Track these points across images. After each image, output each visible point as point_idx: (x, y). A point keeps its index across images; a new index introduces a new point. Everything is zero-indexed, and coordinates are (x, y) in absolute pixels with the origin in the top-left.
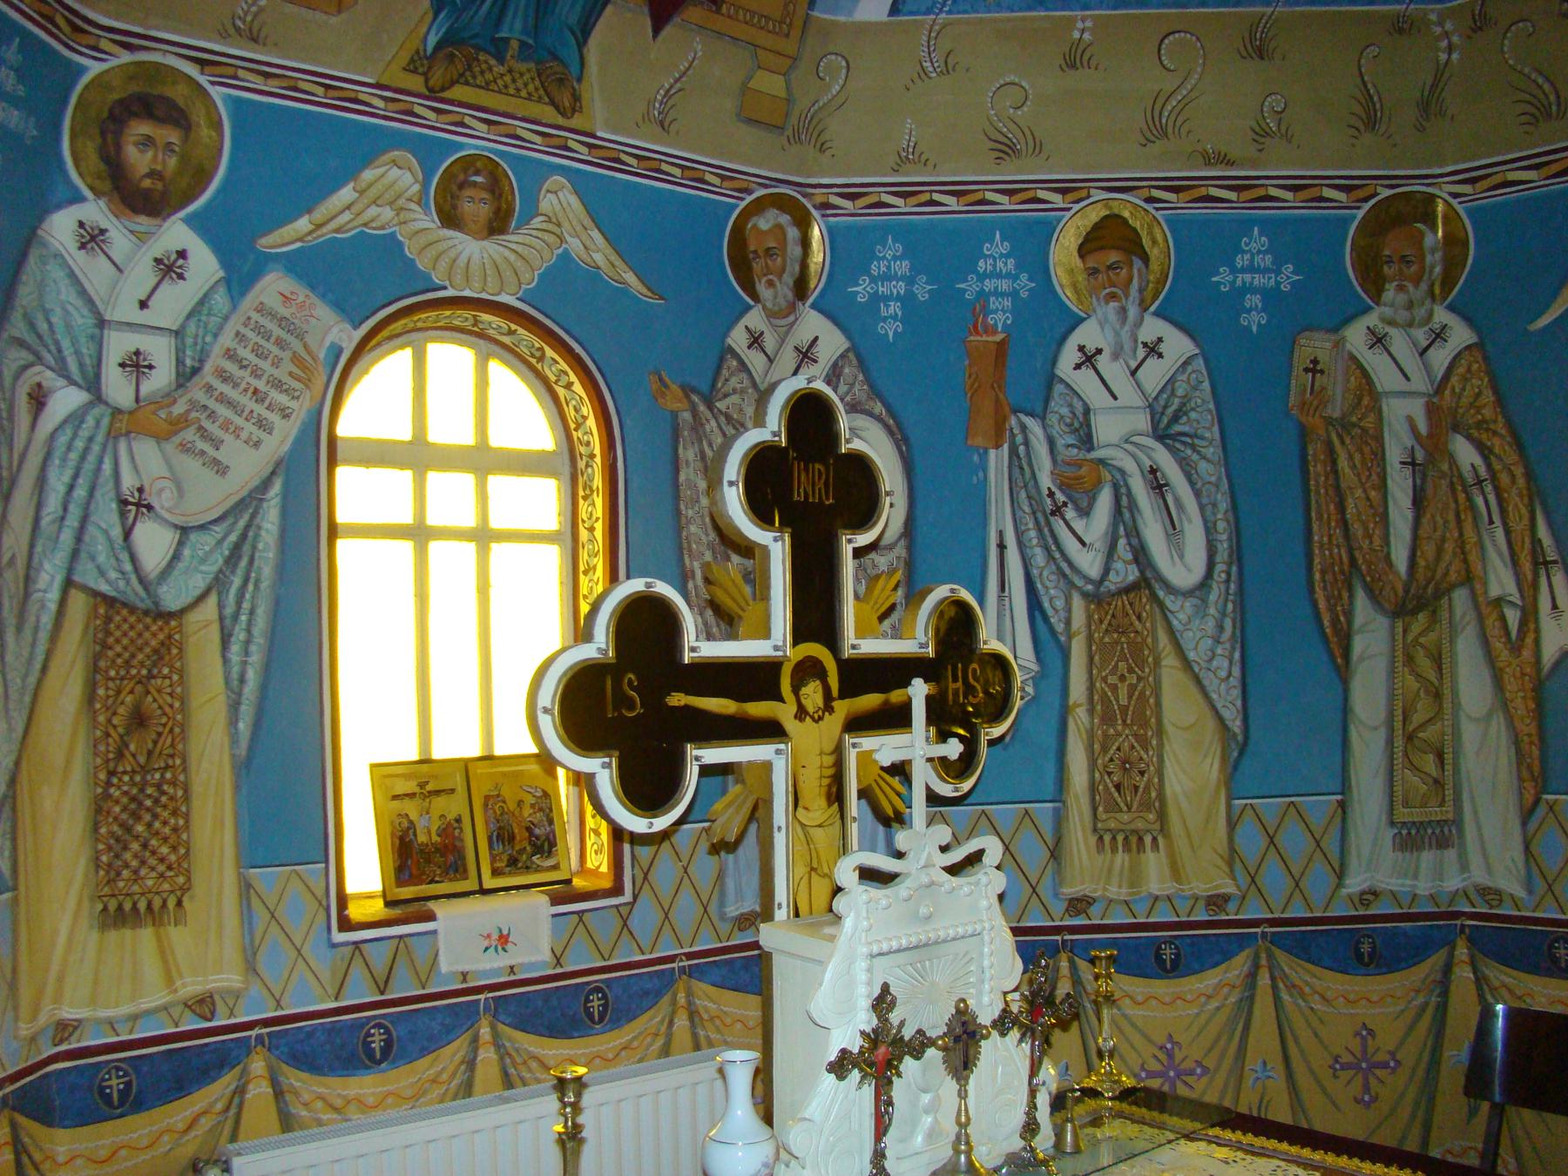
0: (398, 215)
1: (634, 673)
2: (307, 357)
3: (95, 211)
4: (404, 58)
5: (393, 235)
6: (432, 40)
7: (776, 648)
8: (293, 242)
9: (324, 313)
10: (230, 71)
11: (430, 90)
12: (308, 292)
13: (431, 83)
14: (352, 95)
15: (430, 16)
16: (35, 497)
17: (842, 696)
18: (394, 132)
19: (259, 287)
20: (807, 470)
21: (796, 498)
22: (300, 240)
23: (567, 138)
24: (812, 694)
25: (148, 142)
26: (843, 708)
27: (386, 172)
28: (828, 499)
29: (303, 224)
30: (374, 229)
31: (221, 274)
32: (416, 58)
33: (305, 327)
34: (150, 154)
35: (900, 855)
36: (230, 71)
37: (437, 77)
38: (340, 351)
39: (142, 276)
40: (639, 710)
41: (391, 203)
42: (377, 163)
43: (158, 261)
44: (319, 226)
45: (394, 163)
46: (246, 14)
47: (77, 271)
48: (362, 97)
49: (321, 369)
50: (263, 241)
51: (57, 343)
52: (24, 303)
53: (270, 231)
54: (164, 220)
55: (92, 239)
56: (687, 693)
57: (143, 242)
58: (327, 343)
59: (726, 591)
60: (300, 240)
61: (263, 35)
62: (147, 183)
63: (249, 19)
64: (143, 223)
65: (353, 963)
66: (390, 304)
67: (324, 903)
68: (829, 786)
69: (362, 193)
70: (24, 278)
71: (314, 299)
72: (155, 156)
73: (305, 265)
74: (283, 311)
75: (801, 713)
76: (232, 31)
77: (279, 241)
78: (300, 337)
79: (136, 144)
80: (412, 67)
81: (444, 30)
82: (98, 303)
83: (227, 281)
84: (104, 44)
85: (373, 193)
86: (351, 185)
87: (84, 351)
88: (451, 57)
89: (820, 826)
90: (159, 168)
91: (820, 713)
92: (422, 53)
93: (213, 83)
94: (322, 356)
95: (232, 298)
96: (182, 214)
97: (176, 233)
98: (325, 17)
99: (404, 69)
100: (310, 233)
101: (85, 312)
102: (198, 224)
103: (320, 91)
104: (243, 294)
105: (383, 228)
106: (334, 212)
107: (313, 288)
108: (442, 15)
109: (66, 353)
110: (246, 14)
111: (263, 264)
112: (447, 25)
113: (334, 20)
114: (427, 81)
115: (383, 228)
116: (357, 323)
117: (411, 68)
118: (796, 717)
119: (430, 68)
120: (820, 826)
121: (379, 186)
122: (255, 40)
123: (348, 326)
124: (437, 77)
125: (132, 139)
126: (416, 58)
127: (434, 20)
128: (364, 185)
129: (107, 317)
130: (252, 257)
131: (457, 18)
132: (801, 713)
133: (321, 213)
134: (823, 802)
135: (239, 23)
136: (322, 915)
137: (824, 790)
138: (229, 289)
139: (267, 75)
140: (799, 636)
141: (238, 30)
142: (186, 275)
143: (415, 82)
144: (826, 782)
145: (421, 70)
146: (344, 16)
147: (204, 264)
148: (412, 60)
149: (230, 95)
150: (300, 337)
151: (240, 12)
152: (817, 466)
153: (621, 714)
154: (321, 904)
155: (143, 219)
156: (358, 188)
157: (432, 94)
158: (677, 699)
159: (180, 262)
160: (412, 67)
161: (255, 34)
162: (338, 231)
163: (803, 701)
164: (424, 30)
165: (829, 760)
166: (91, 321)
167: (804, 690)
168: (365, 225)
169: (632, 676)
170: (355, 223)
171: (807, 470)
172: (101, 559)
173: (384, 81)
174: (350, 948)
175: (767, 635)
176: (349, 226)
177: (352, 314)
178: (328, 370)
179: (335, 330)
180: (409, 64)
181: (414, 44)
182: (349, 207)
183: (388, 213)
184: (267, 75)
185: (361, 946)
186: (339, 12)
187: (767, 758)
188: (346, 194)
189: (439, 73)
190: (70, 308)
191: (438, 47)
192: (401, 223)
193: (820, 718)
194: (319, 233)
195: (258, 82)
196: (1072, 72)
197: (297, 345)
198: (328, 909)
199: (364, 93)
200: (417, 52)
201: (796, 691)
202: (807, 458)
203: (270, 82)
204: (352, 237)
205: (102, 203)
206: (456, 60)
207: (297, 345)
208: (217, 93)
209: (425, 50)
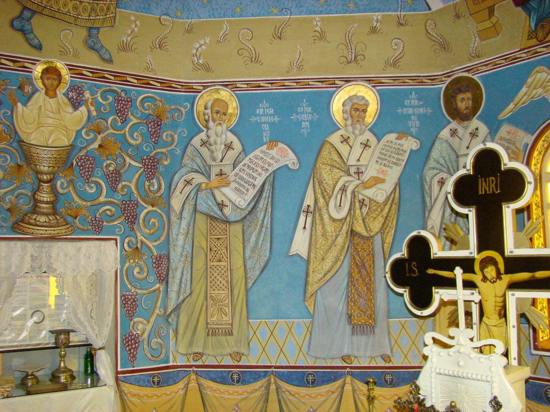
0: (544, 89)
1: (415, 261)
2: (516, 150)
3: (454, 125)
4: (526, 36)
5: (544, 97)
6: (533, 25)
7: (471, 253)
8: (508, 113)
9: (521, 133)
10: (476, 69)
11: (540, 41)
12: (515, 128)
13: (539, 39)
14: (514, 57)
15: (528, 17)
16: (442, 210)
17: (506, 272)
18: (533, 62)
19: (499, 132)
20: (485, 181)
21: (480, 193)
22: (511, 111)
23: (536, 49)
24: (490, 272)
25: (463, 99)
26: (507, 279)
27: (535, 77)
28: (497, 190)
29: (511, 106)
30: (537, 97)
31: (488, 131)
32: (530, 34)
33: (515, 140)
34: (464, 103)
35: (452, 338)
36: (476, 69)
37: (541, 35)
38: (528, 145)
39: (467, 138)
40: (417, 274)
41: (541, 86)
42: (532, 75)
43: (471, 133)
44: (516, 105)
45: (538, 72)
46: (473, 51)
47: (451, 143)
48: (517, 56)
49: (521, 153)
50: (500, 116)
51: (447, 165)
52: (434, 157)
53: (500, 114)
54: (471, 120)
55: (454, 133)
56: (435, 269)
57: (466, 129)
58: (523, 143)
59: (453, 233)
60: (511, 111)
61: (480, 54)
62: (465, 111)
63: (474, 52)
64: (466, 123)
65: (540, 362)
66: (544, 123)
67: (528, 338)
68: (500, 310)
69: (529, 87)
70: (433, 150)
71: (518, 130)
72: (466, 103)
73: (513, 120)
74: (508, 137)
75: (485, 279)
76: (471, 58)
77: (505, 114)
78: (514, 144)
79: (460, 102)
80: (530, 38)
81: (535, 19)
82: (456, 150)
83: (490, 133)
84: (443, 79)
85: (532, 86)
86: (525, 86)
87: (454, 165)
88: (543, 26)
89: (495, 326)
90: (467, 106)
91: (495, 280)
92: (531, 31)
93: (473, 75)
94: (521, 148)
95: (492, 138)
96: (475, 117)
97: (475, 123)
98: (495, 39)
99: (528, 40)
100: (514, 108)
101: (454, 154)
102: (480, 118)
103: (504, 61)
104: (495, 135)
105: (539, 96)
106: (521, 98)
107: (517, 126)
108: (532, 15)
109: (450, 167)
110: (473, 51)
111: (499, 124)
112: (536, 15)
113: (498, 38)
114: (537, 39)
115: (539, 96)
116: (533, 133)
117: (530, 38)
118: (482, 280)
119: (536, 35)
120: (495, 326)
121: (535, 82)
122: (479, 57)
123: (530, 136)
124: (541, 35)
125: (459, 101)
126: (530, 34)
127: (530, 17)
128: (529, 84)
129: (459, 154)
130: (497, 122)
131: (538, 12)
132: (485, 279)
133: (516, 101)
134: (497, 317)
135: (472, 55)
136: (527, 343)
137: (497, 312)
138: (491, 135)
139: (486, 65)
140: (480, 249)
141: (472, 56)
142: (478, 135)
143: (534, 42)
144: (498, 308)
145: (533, 37)
146: (500, 35)
147: (483, 129)
148: (529, 35)
149: (479, 76)
150: (514, 144)
151: (472, 52)
152: (491, 178)
153: (411, 275)
154: (527, 338)
155: (465, 122)
156: (527, 86)
157: (541, 42)
158: (431, 271)
159: (477, 131)
160: (530, 38)
161: (477, 55)
162: (522, 104)
163: (486, 274)
164: (528, 23)
165: (501, 299)
166: (455, 157)
167: (485, 270)
168: (532, 98)
169: (414, 263)
170: (529, 99)
171: (485, 181)
172: (461, 225)
173: (522, 48)
174: (538, 357)
175: (468, 248)
176: (527, 100)
177: (529, 130)
178: (524, 153)
179: (525, 138)
180: (528, 37)
181: (527, 30)
182: (525, 94)
183: (540, 90)
184: (486, 65)
185: (543, 357)
186: (498, 35)
187: (515, 299)
188: (524, 90)
189: (541, 34)
190: (450, 154)
191: (536, 26)
192: (546, 92)
193: (494, 282)
194: (517, 107)
195: (485, 68)
196: (373, 34)
197: (513, 147)
198: (530, 341)
199: (518, 55)
200: (529, 31)
201: (482, 270)
202: (485, 176)
203: (488, 66)
204: (529, 104)
205: (455, 122)
206: (545, 26)
207: (513, 147)
208: (475, 77)
209: (532, 29)
